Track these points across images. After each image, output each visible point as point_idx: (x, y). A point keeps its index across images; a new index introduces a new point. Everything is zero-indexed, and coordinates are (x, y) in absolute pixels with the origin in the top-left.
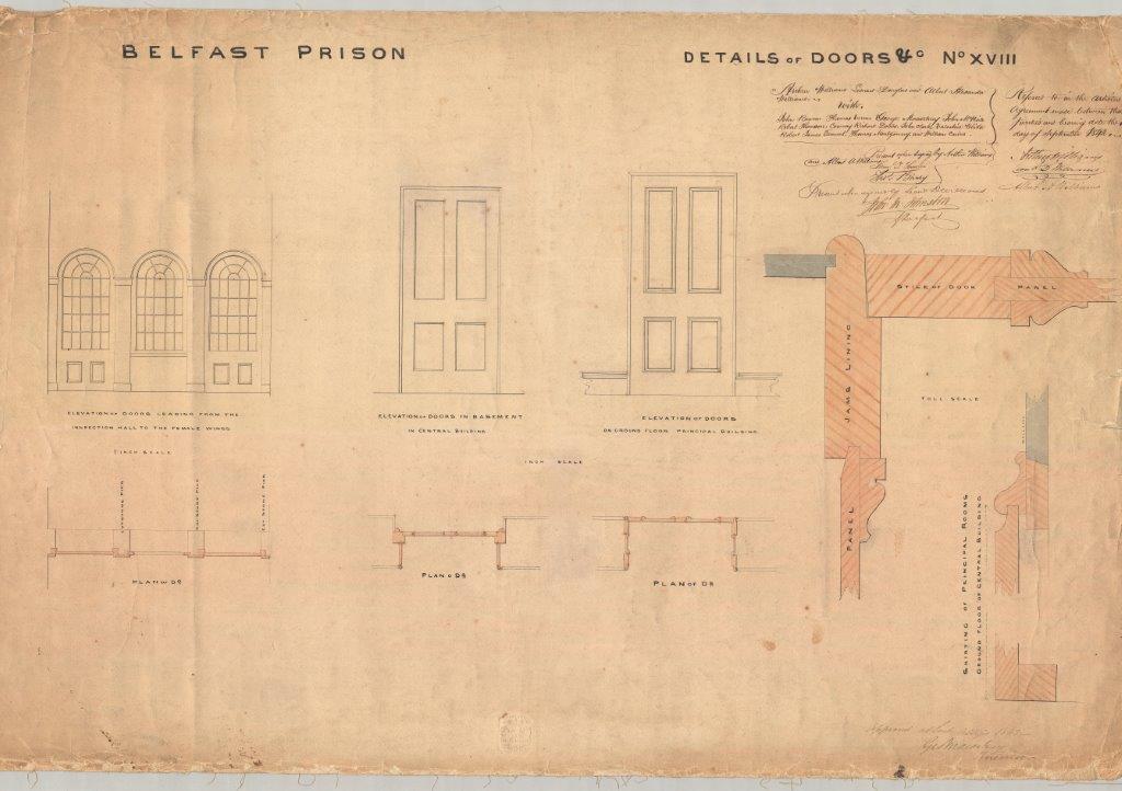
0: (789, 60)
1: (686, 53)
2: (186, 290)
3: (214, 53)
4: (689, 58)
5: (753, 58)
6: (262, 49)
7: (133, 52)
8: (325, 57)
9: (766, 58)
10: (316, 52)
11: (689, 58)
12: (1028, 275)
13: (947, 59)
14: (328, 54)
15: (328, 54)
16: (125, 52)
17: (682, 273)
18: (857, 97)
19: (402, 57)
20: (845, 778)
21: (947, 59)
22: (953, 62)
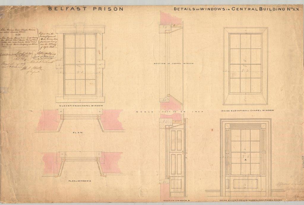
0: (197, 9)
1: (175, 8)
2: (224, 156)
3: (72, 9)
4: (175, 9)
5: (189, 9)
6: (85, 8)
7: (51, 8)
8: (279, 10)
9: (272, 9)
10: (98, 8)
11: (175, 9)
12: (174, 125)
13: (120, 9)
14: (250, 9)
15: (250, 9)
16: (260, 9)
17: (176, 147)
18: (20, 33)
19: (242, 10)
20: (290, 5)
21: (120, 9)
22: (290, 10)
